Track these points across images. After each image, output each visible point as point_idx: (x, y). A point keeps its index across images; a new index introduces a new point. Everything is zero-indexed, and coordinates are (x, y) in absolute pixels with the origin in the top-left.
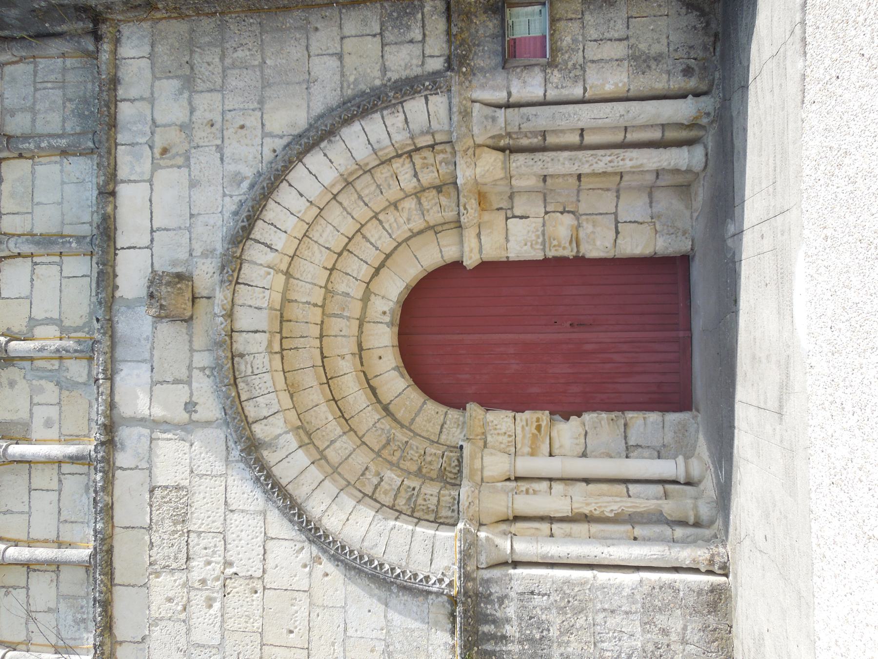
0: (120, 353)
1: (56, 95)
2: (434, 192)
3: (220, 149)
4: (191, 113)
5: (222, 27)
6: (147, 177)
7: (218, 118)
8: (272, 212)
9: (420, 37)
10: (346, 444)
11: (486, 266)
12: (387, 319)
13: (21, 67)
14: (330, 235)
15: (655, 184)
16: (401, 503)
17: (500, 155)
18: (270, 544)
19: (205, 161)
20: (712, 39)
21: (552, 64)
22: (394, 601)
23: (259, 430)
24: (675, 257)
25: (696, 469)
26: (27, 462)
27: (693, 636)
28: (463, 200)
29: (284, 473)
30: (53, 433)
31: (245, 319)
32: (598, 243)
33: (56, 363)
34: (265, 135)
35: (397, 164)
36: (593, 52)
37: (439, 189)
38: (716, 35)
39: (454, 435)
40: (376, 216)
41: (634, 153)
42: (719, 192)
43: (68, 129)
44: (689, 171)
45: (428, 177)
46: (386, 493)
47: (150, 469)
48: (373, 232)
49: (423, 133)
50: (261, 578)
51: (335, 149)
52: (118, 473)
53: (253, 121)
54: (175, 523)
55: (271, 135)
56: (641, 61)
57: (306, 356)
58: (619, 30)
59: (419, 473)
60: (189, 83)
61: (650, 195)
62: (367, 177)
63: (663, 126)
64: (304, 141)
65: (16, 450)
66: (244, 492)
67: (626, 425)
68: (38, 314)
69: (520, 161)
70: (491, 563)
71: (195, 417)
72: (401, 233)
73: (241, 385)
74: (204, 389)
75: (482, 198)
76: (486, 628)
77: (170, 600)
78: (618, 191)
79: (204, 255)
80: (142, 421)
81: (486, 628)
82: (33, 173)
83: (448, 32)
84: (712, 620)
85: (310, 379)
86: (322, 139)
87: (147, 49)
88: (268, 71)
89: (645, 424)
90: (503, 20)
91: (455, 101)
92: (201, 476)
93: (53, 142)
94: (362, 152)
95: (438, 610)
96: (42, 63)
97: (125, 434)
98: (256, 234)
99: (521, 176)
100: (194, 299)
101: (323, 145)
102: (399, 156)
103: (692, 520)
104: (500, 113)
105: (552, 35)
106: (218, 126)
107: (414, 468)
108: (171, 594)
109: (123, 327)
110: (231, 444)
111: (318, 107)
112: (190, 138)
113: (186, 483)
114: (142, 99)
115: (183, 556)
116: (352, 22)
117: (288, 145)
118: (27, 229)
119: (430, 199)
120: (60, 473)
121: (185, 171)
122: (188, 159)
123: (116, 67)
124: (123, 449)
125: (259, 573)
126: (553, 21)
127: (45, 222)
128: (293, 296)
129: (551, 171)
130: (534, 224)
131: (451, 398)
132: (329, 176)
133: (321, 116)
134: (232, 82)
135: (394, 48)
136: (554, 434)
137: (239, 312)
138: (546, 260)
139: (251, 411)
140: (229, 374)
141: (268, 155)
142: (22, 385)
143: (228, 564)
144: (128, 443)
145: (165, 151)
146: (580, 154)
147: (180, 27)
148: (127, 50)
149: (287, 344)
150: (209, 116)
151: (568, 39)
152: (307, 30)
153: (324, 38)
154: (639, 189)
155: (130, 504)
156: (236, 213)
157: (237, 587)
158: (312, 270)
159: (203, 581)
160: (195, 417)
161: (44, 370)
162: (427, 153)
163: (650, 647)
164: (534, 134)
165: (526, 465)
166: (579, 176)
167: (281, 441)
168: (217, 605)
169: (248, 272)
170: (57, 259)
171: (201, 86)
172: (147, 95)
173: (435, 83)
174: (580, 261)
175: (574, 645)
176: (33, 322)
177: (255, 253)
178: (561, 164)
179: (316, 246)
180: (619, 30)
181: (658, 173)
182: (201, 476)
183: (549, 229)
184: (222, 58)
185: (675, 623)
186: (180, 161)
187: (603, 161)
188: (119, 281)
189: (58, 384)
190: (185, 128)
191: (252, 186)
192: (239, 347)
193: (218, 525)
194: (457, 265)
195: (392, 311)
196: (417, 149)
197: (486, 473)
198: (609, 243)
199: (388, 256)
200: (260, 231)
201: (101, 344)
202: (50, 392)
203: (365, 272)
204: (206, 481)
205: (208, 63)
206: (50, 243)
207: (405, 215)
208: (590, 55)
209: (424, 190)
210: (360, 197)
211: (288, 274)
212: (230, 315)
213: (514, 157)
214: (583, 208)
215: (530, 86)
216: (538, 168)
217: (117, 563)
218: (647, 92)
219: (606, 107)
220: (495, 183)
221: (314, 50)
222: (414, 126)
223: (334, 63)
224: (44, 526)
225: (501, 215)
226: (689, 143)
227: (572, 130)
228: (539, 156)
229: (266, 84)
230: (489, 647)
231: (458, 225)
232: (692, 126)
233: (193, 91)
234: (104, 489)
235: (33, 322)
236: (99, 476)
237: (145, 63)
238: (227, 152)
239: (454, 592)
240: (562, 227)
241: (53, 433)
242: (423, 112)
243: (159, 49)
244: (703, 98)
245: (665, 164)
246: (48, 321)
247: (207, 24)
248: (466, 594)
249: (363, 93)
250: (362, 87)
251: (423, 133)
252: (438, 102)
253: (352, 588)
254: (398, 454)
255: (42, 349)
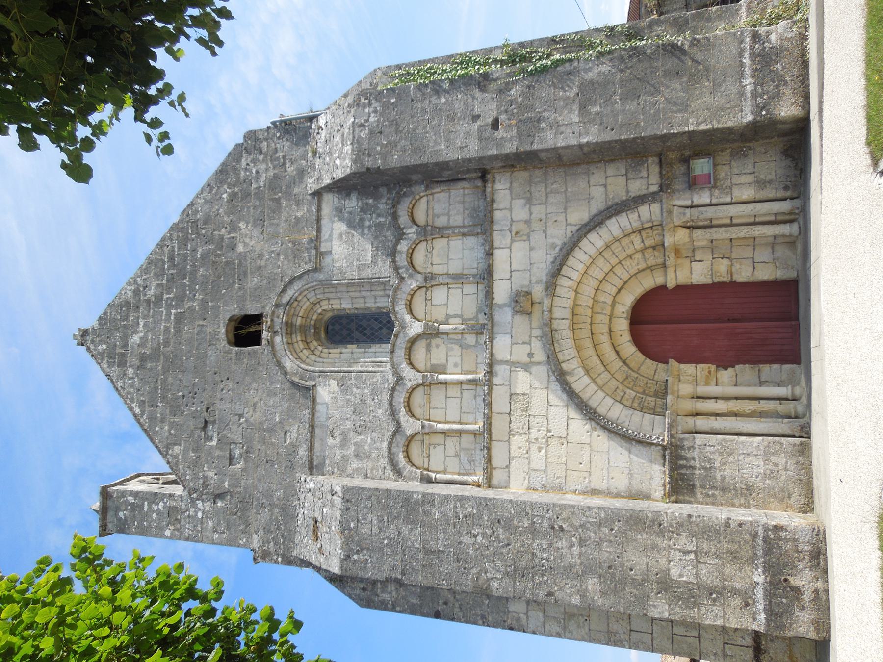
0: (496, 330)
1: (460, 207)
2: (651, 250)
3: (545, 232)
4: (531, 215)
5: (545, 174)
6: (508, 246)
7: (544, 217)
8: (571, 261)
9: (646, 175)
10: (606, 376)
11: (679, 288)
12: (625, 315)
13: (442, 194)
14: (597, 273)
15: (774, 243)
16: (636, 405)
17: (687, 231)
18: (570, 421)
19: (537, 238)
20: (799, 172)
21: (715, 187)
22: (633, 449)
23: (565, 366)
24: (789, 281)
25: (798, 391)
26: (446, 383)
27: (791, 466)
28: (667, 253)
29: (577, 387)
30: (458, 370)
31: (557, 313)
32: (743, 274)
33: (460, 337)
34: (567, 225)
35: (633, 236)
36: (736, 180)
37: (654, 248)
38: (801, 170)
39: (662, 375)
40: (620, 262)
41: (760, 228)
42: (800, 245)
43: (466, 223)
44: (791, 236)
45: (648, 243)
46: (627, 400)
47: (510, 385)
48: (619, 270)
49: (648, 222)
50: (566, 438)
51: (603, 231)
52: (494, 387)
53: (561, 218)
54: (523, 411)
55: (570, 225)
56: (761, 184)
57: (585, 333)
58: (750, 168)
59: (644, 393)
60: (529, 201)
61: (773, 248)
62: (617, 243)
63: (776, 214)
64: (588, 227)
65: (442, 377)
66: (557, 398)
67: (759, 370)
68: (451, 312)
69: (698, 233)
70: (685, 431)
71: (533, 360)
72: (633, 271)
73: (556, 345)
74: (537, 345)
75: (677, 252)
76: (681, 462)
77: (520, 448)
78: (754, 246)
79: (537, 283)
80: (506, 362)
81: (681, 462)
82: (448, 245)
83: (661, 173)
84: (801, 459)
85: (588, 343)
86: (596, 226)
87: (508, 185)
88: (568, 194)
89: (770, 370)
90: (689, 167)
91: (664, 206)
92: (536, 389)
93: (461, 230)
94: (617, 232)
95: (656, 452)
96: (453, 192)
97: (498, 368)
98: (563, 272)
99: (699, 240)
100: (532, 303)
101: (597, 228)
102: (634, 232)
103: (793, 415)
104: (688, 211)
105: (714, 173)
106: (544, 221)
107: (641, 390)
108: (520, 445)
109: (497, 318)
110: (551, 373)
111: (594, 211)
112: (529, 227)
113: (528, 392)
114: (506, 209)
115: (526, 427)
116: (611, 170)
117: (579, 229)
118: (445, 271)
119: (649, 253)
120: (461, 389)
121: (527, 242)
122: (529, 237)
123: (493, 194)
124: (497, 375)
125: (565, 435)
126: (715, 165)
127: (455, 267)
128: (579, 302)
129: (715, 238)
130: (706, 265)
131: (661, 359)
132: (600, 244)
133: (596, 215)
134: (551, 200)
135: (633, 181)
136: (719, 375)
137: (555, 310)
138: (714, 284)
139: (561, 357)
140: (550, 338)
141: (569, 234)
142: (443, 347)
143: (549, 431)
144: (499, 373)
145: (517, 233)
146: (731, 229)
147: (525, 174)
148: (498, 186)
149: (576, 326)
150: (539, 216)
151: (723, 174)
152: (588, 174)
153: (597, 177)
154: (766, 244)
155: (500, 402)
156: (553, 262)
157: (554, 442)
158: (588, 290)
159: (536, 439)
160: (533, 360)
161: (454, 339)
162: (649, 231)
163: (768, 472)
164: (706, 220)
165: (702, 390)
166: (731, 240)
167: (576, 371)
168: (543, 451)
169: (559, 291)
170: (460, 286)
171: (535, 202)
172: (508, 207)
173: (654, 198)
174: (733, 284)
175: (728, 471)
176: (448, 317)
177: (562, 281)
178: (720, 234)
179: (590, 278)
180: (750, 168)
181: (775, 237)
182: (536, 389)
183: (715, 267)
184: (546, 188)
185: (781, 460)
186: (525, 238)
187: (743, 232)
188: (494, 296)
189: (460, 346)
190: (528, 222)
191: (561, 250)
192: (555, 326)
193: (544, 413)
194: (663, 288)
195: (627, 311)
196: (644, 229)
197: (680, 393)
198: (749, 273)
199: (625, 283)
200: (565, 270)
201: (484, 327)
202: (457, 350)
203: (614, 290)
204: (538, 391)
205: (539, 191)
206: (459, 278)
207: (636, 261)
208: (734, 181)
209: (646, 248)
210: (614, 253)
211: (576, 292)
212: (550, 311)
213: (695, 231)
214: (734, 256)
215: (704, 197)
216: (708, 236)
217: (493, 430)
218: (765, 198)
219: (744, 206)
220: (684, 244)
221: (592, 183)
222: (643, 219)
223: (602, 189)
224: (453, 415)
225: (688, 261)
226: (791, 221)
227: (726, 218)
228: (708, 230)
229: (567, 200)
230: (683, 471)
231: (664, 266)
232: (790, 213)
233: (531, 205)
234: (488, 394)
235: (448, 317)
236: (486, 388)
237: (507, 192)
238: (549, 233)
239: (665, 444)
240: (722, 266)
241: (458, 370)
242: (648, 212)
243: (514, 185)
244: (795, 200)
245: (777, 233)
246: (456, 316)
247: (538, 172)
248: (671, 444)
249: (617, 204)
250: (617, 200)
251: (648, 222)
252: (656, 207)
253: (611, 443)
254: (632, 383)
255: (456, 329)
